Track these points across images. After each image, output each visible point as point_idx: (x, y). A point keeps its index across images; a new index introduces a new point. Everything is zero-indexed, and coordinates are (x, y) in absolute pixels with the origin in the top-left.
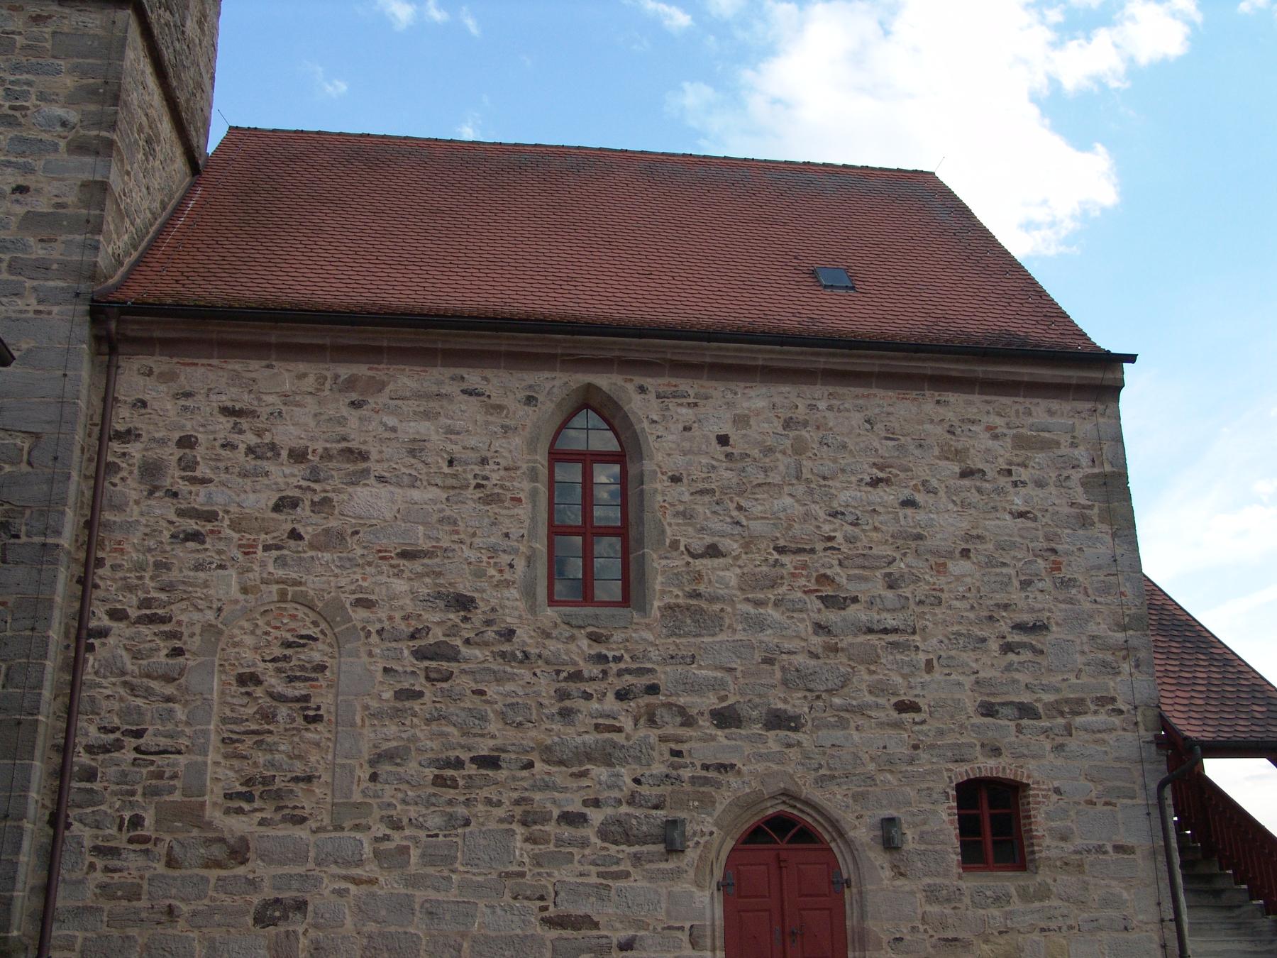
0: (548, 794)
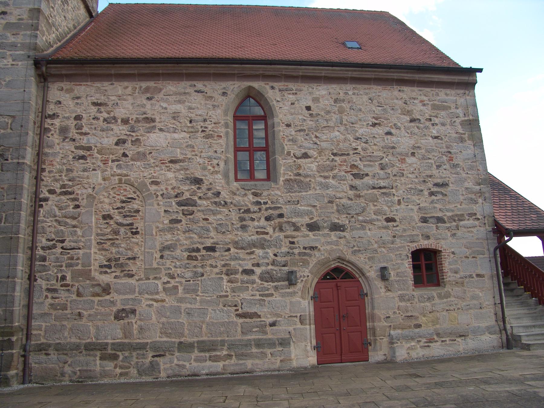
0: (237, 262)
